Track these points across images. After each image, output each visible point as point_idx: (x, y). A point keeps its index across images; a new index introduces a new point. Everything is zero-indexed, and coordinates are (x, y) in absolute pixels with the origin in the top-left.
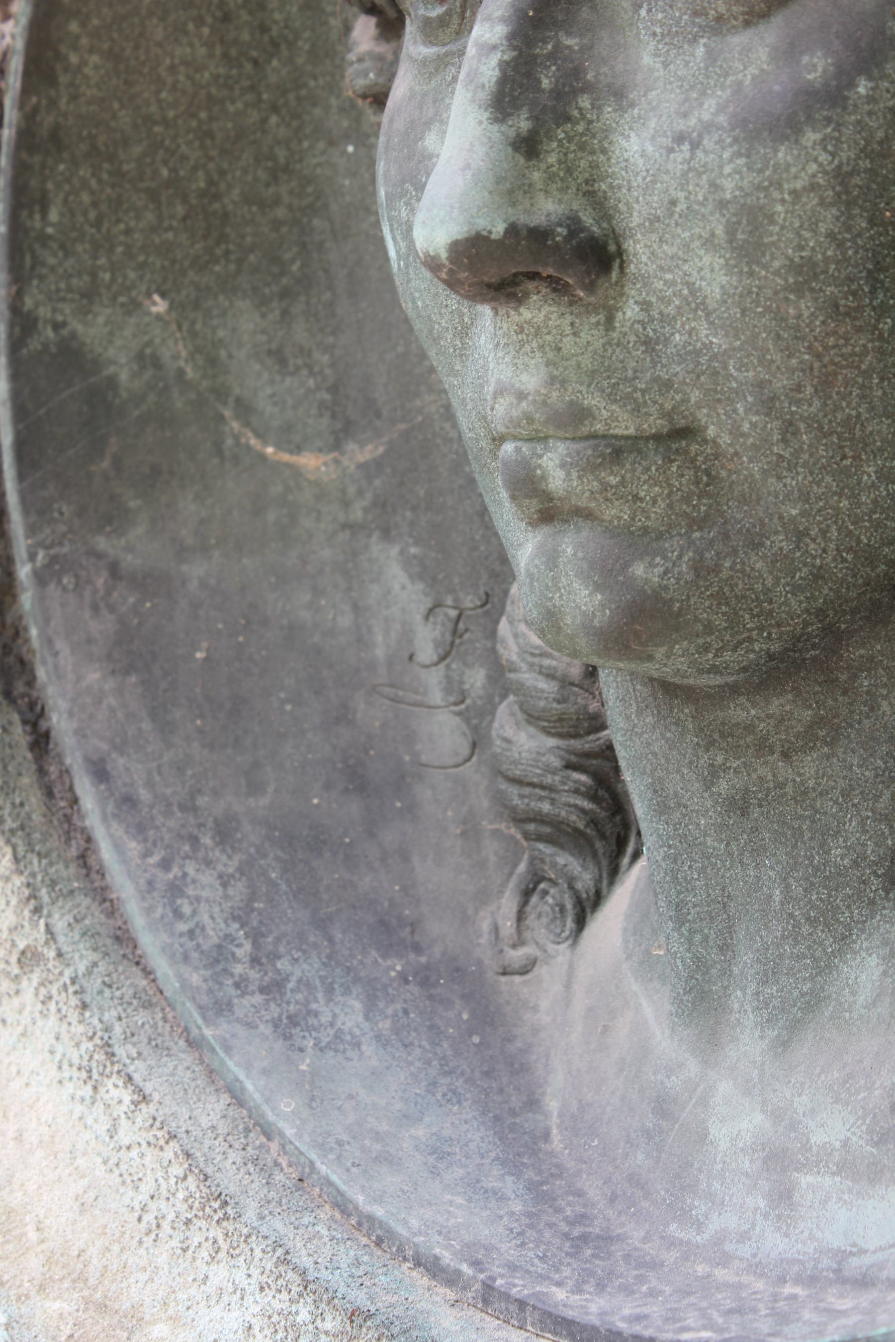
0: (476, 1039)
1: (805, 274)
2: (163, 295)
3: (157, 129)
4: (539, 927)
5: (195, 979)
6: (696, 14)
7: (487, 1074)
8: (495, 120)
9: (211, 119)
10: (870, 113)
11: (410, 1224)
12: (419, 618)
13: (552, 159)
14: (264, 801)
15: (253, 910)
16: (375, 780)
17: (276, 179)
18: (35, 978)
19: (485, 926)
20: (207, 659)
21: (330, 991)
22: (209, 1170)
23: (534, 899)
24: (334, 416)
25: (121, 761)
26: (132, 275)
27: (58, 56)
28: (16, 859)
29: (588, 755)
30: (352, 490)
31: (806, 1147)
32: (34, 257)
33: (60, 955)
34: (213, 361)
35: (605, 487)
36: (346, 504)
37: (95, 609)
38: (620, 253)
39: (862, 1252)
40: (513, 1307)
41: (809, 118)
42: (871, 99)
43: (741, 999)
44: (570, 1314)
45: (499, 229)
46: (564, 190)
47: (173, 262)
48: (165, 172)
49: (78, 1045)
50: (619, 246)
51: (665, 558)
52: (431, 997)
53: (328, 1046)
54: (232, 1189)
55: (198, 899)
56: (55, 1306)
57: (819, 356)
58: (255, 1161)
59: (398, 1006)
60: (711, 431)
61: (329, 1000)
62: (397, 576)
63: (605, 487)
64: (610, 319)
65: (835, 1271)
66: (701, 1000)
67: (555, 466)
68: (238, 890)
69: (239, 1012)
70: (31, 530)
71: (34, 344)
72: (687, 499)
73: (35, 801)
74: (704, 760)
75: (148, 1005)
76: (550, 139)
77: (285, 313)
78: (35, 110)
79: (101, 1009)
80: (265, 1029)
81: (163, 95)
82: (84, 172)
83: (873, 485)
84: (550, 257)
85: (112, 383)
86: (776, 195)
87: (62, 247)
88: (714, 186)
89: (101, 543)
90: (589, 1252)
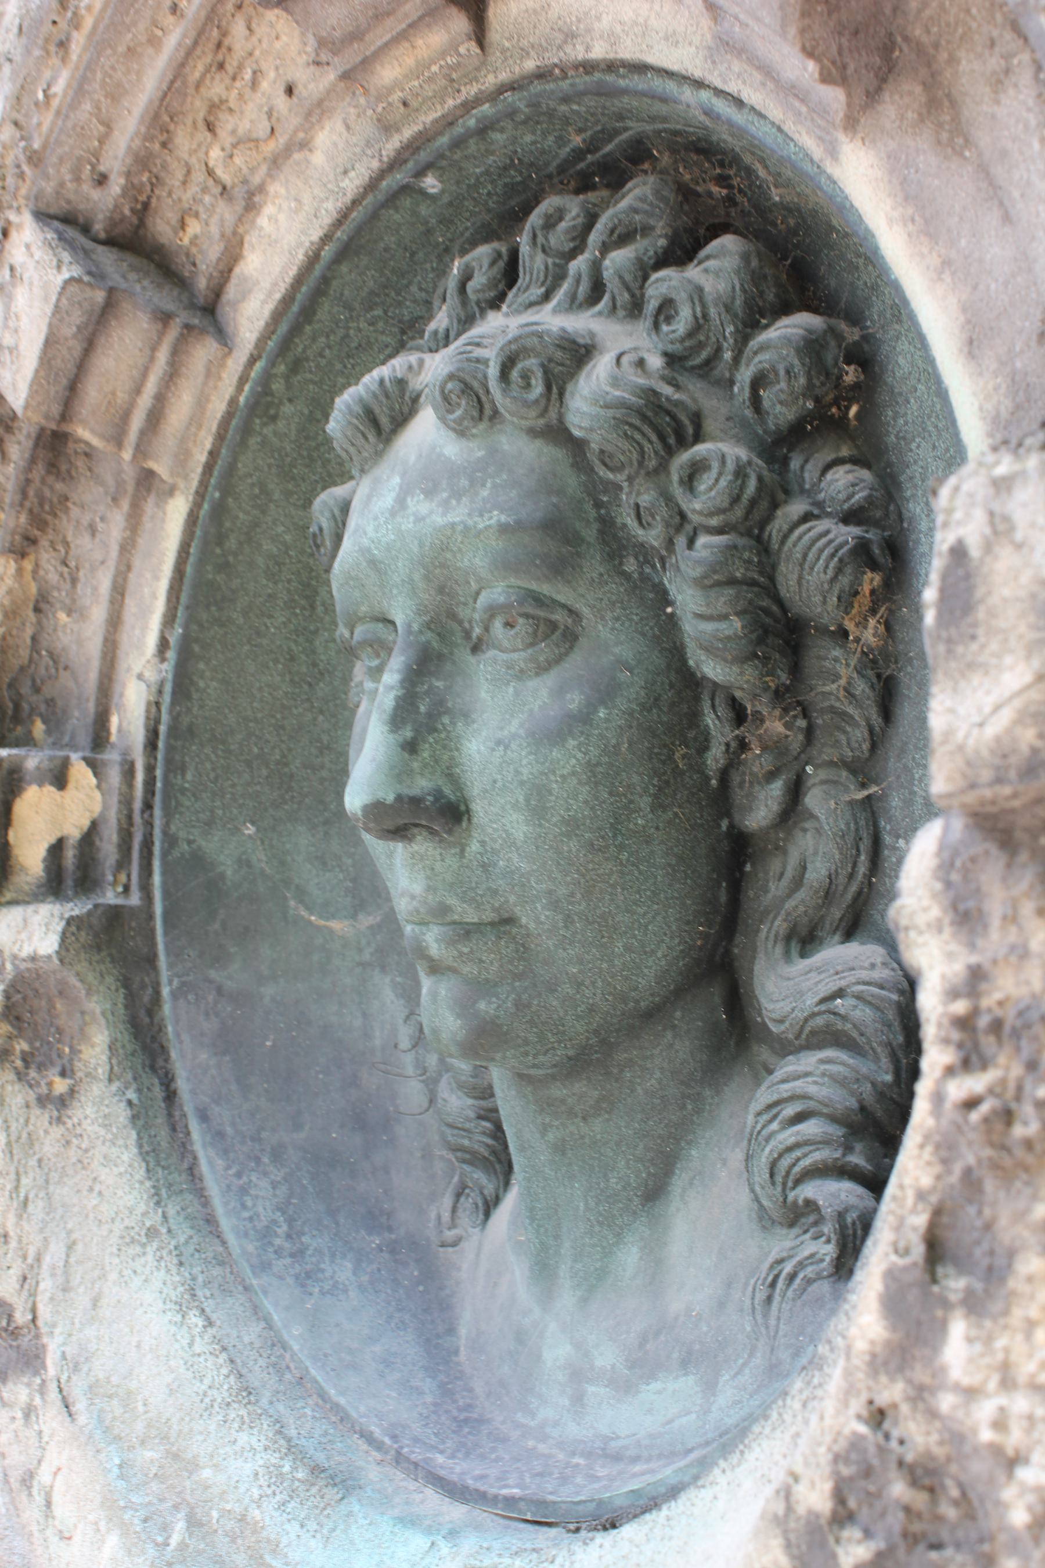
0: (421, 1288)
1: (572, 826)
2: (253, 823)
3: (251, 724)
4: (465, 1218)
5: (250, 1248)
6: (508, 668)
7: (425, 1311)
8: (392, 731)
9: (284, 718)
10: (607, 729)
11: (359, 1410)
12: (401, 1021)
13: (426, 754)
14: (302, 1135)
15: (290, 1203)
16: (371, 1122)
17: (322, 753)
18: (155, 1245)
19: (433, 1215)
20: (273, 1046)
21: (333, 1256)
22: (244, 1371)
23: (462, 1199)
24: (354, 897)
25: (217, 1109)
26: (235, 811)
27: (192, 683)
28: (148, 1171)
30: (364, 941)
32: (177, 802)
33: (169, 1231)
34: (282, 863)
35: (461, 954)
36: (360, 950)
37: (207, 1014)
38: (468, 811)
39: (618, 1437)
40: (412, 1467)
41: (571, 733)
42: (607, 720)
43: (563, 1270)
44: (442, 1473)
45: (390, 798)
46: (433, 773)
47: (260, 803)
48: (256, 750)
49: (175, 1289)
50: (467, 806)
51: (498, 998)
52: (396, 1261)
53: (328, 1292)
54: (257, 1384)
55: (257, 1197)
56: (149, 1454)
57: (583, 876)
58: (274, 1365)
59: (375, 1266)
60: (524, 920)
61: (332, 1262)
63: (461, 954)
64: (463, 851)
65: (603, 1449)
66: (543, 1270)
67: (433, 939)
68: (283, 1191)
69: (275, 1270)
70: (171, 966)
71: (176, 853)
72: (511, 962)
73: (164, 1133)
74: (539, 1120)
75: (222, 1264)
76: (424, 742)
77: (326, 833)
78: (179, 714)
79: (191, 1266)
80: (290, 1280)
81: (255, 704)
82: (208, 750)
83: (622, 955)
84: (435, 813)
85: (222, 876)
86: (553, 778)
87: (194, 795)
88: (517, 772)
89: (212, 974)
90: (467, 1430)
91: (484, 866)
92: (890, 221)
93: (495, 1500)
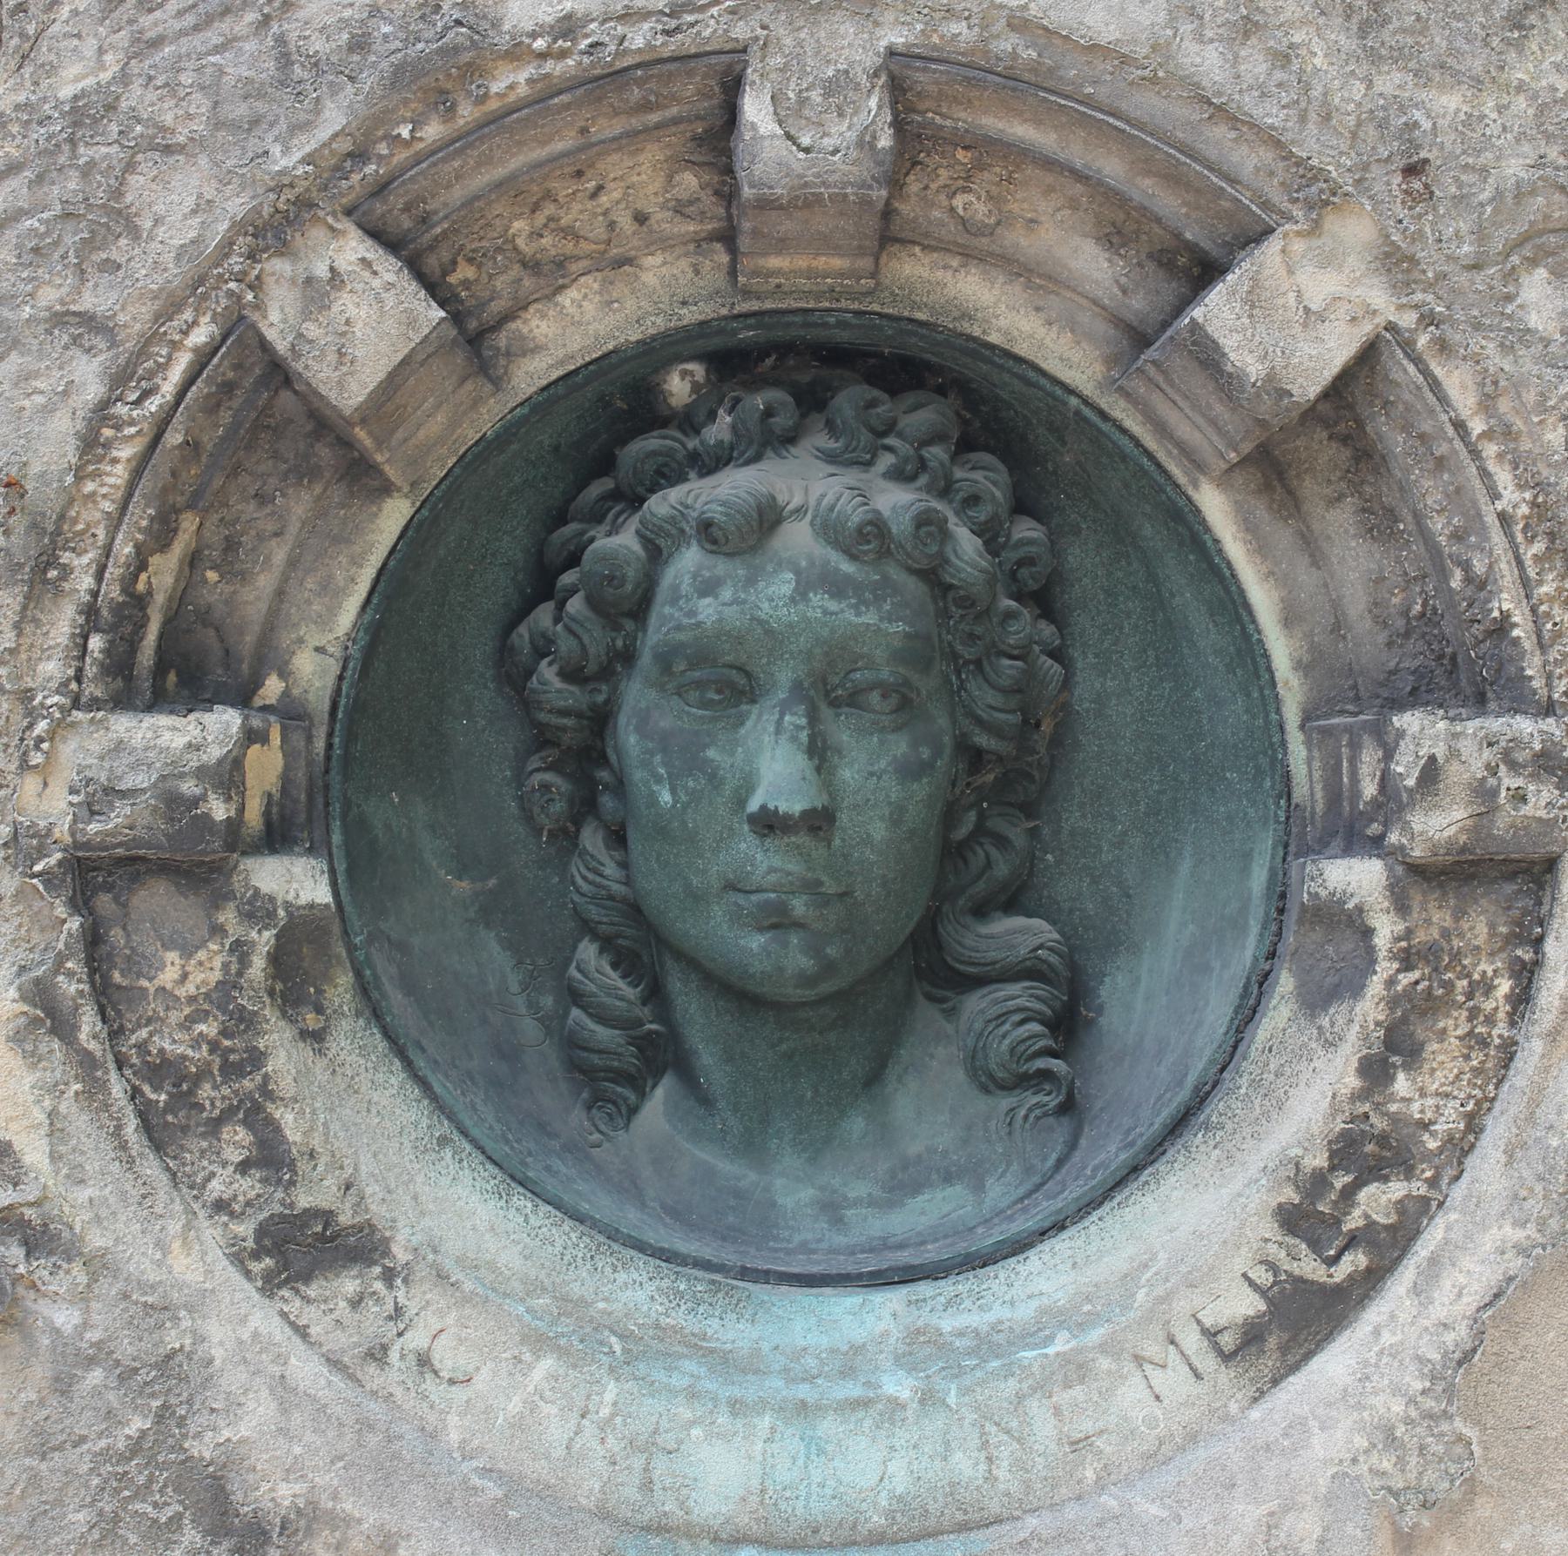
29: (635, 1038)
31: (846, 1198)
62: (495, 947)
88: (888, 796)
91: (844, 856)
92: (1235, 538)
93: (860, 1276)
